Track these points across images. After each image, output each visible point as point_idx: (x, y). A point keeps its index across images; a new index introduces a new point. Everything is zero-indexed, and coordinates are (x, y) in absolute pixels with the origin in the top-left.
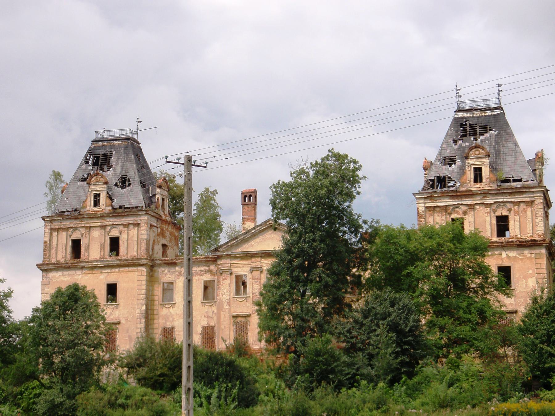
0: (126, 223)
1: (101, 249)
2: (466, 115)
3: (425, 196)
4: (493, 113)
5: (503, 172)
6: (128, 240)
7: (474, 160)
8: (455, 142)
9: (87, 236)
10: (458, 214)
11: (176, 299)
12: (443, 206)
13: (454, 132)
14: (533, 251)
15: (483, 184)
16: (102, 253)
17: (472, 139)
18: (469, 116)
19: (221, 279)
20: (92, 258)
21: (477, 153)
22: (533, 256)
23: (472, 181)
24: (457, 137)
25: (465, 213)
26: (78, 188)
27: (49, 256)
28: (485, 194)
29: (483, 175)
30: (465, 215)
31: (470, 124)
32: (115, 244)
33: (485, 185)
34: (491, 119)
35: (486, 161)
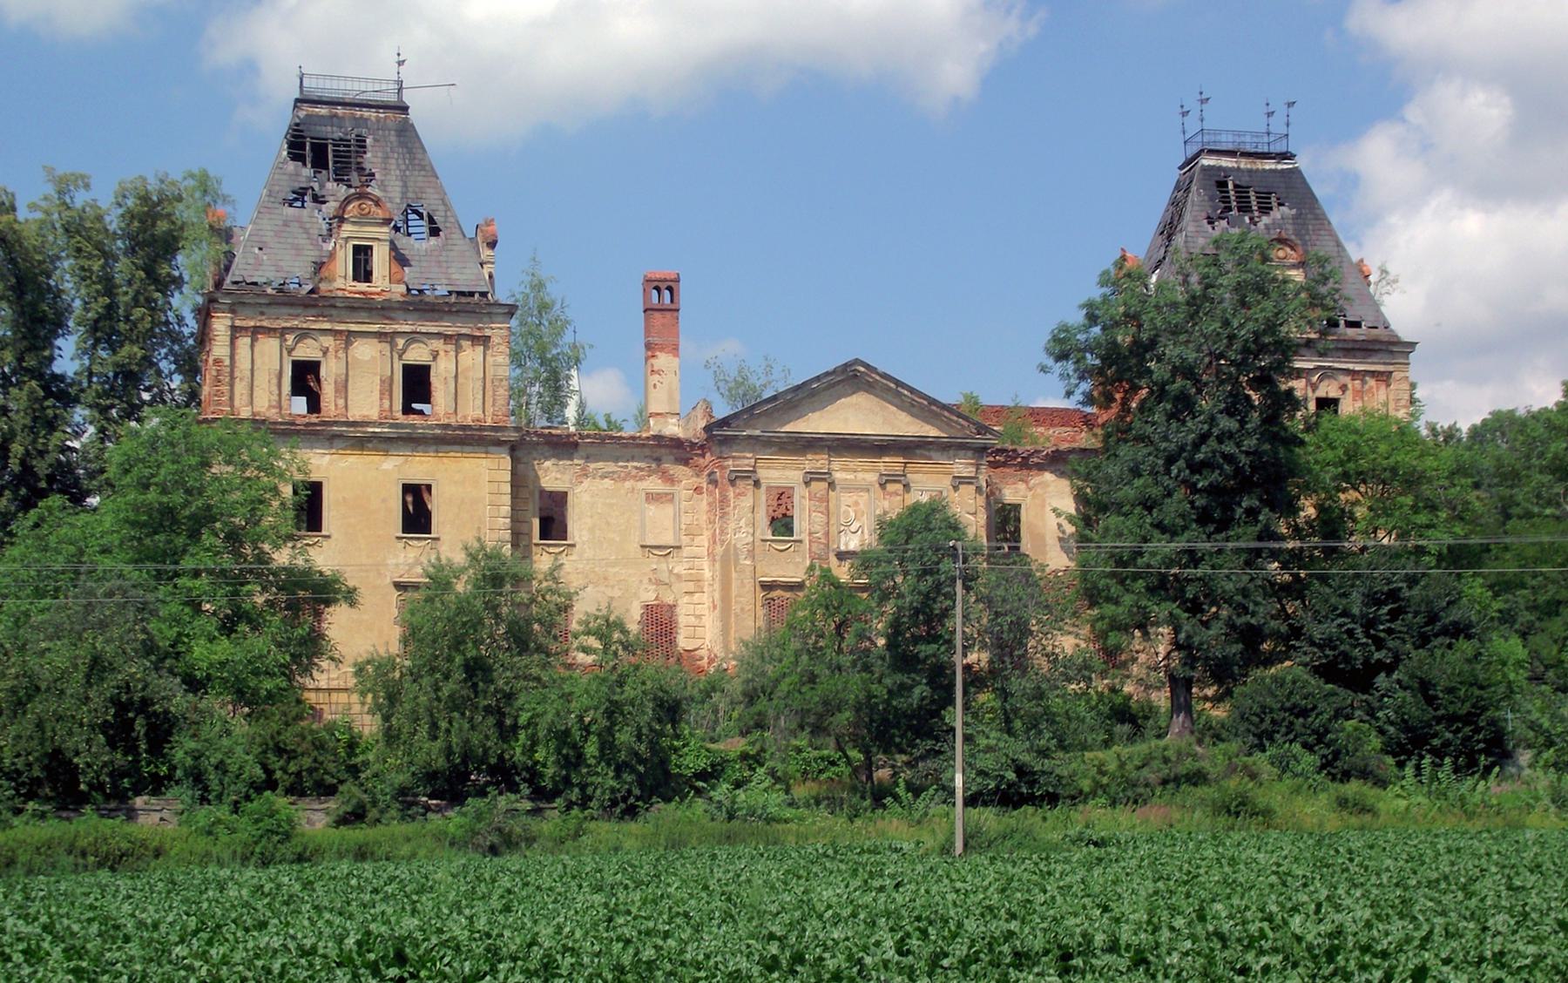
1: (382, 393)
4: (1280, 167)
6: (456, 377)
8: (1211, 221)
9: (341, 354)
11: (576, 534)
16: (387, 403)
17: (1247, 219)
19: (731, 494)
20: (355, 414)
26: (286, 224)
27: (232, 399)
31: (1236, 186)
32: (417, 384)
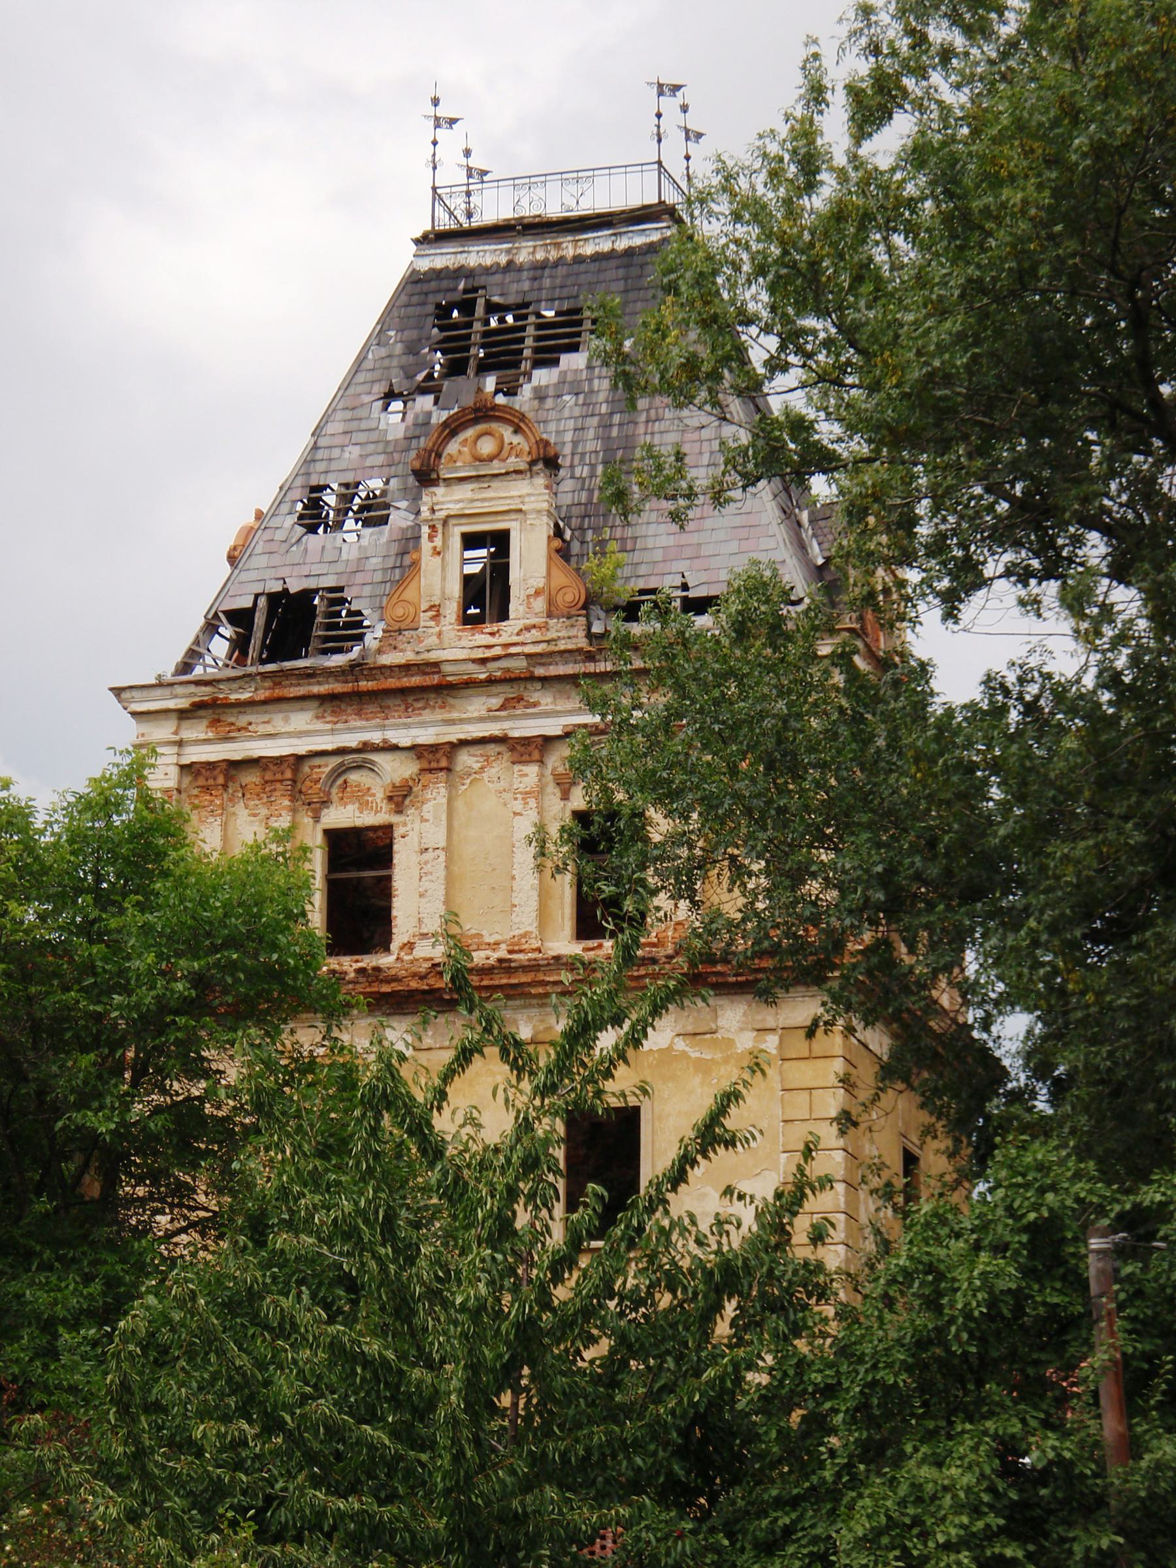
2: (480, 255)
3: (183, 703)
4: (622, 244)
5: (636, 557)
7: (464, 492)
10: (364, 806)
12: (279, 761)
13: (399, 349)
14: (769, 1017)
15: (508, 631)
18: (488, 261)
21: (487, 447)
22: (771, 1043)
23: (452, 610)
24: (410, 377)
25: (400, 797)
28: (515, 682)
29: (515, 575)
30: (399, 810)
33: (525, 624)
34: (610, 275)
35: (532, 493)
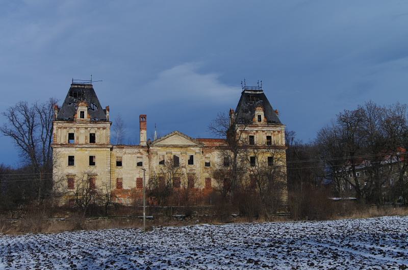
0: (99, 127)
32: (92, 138)
